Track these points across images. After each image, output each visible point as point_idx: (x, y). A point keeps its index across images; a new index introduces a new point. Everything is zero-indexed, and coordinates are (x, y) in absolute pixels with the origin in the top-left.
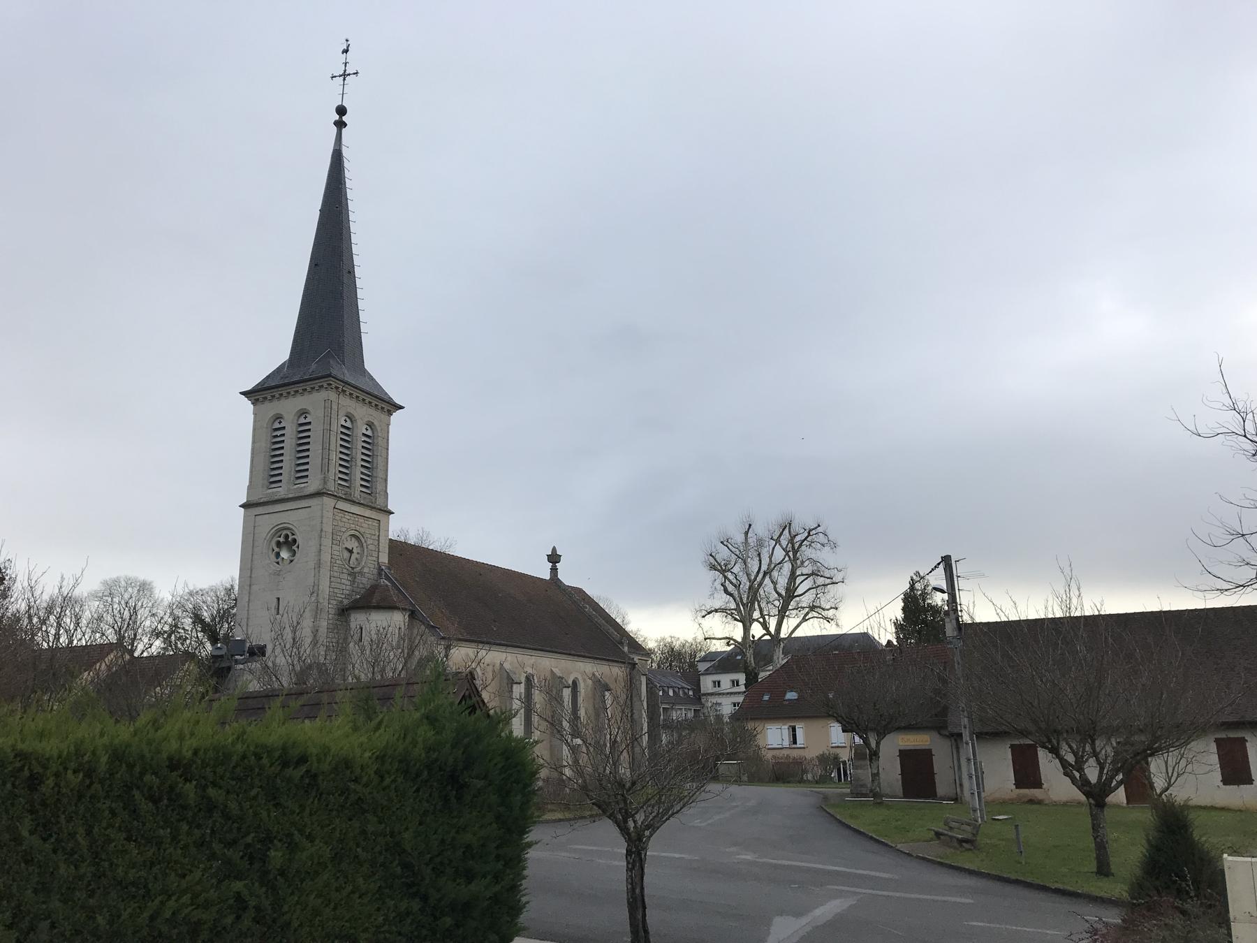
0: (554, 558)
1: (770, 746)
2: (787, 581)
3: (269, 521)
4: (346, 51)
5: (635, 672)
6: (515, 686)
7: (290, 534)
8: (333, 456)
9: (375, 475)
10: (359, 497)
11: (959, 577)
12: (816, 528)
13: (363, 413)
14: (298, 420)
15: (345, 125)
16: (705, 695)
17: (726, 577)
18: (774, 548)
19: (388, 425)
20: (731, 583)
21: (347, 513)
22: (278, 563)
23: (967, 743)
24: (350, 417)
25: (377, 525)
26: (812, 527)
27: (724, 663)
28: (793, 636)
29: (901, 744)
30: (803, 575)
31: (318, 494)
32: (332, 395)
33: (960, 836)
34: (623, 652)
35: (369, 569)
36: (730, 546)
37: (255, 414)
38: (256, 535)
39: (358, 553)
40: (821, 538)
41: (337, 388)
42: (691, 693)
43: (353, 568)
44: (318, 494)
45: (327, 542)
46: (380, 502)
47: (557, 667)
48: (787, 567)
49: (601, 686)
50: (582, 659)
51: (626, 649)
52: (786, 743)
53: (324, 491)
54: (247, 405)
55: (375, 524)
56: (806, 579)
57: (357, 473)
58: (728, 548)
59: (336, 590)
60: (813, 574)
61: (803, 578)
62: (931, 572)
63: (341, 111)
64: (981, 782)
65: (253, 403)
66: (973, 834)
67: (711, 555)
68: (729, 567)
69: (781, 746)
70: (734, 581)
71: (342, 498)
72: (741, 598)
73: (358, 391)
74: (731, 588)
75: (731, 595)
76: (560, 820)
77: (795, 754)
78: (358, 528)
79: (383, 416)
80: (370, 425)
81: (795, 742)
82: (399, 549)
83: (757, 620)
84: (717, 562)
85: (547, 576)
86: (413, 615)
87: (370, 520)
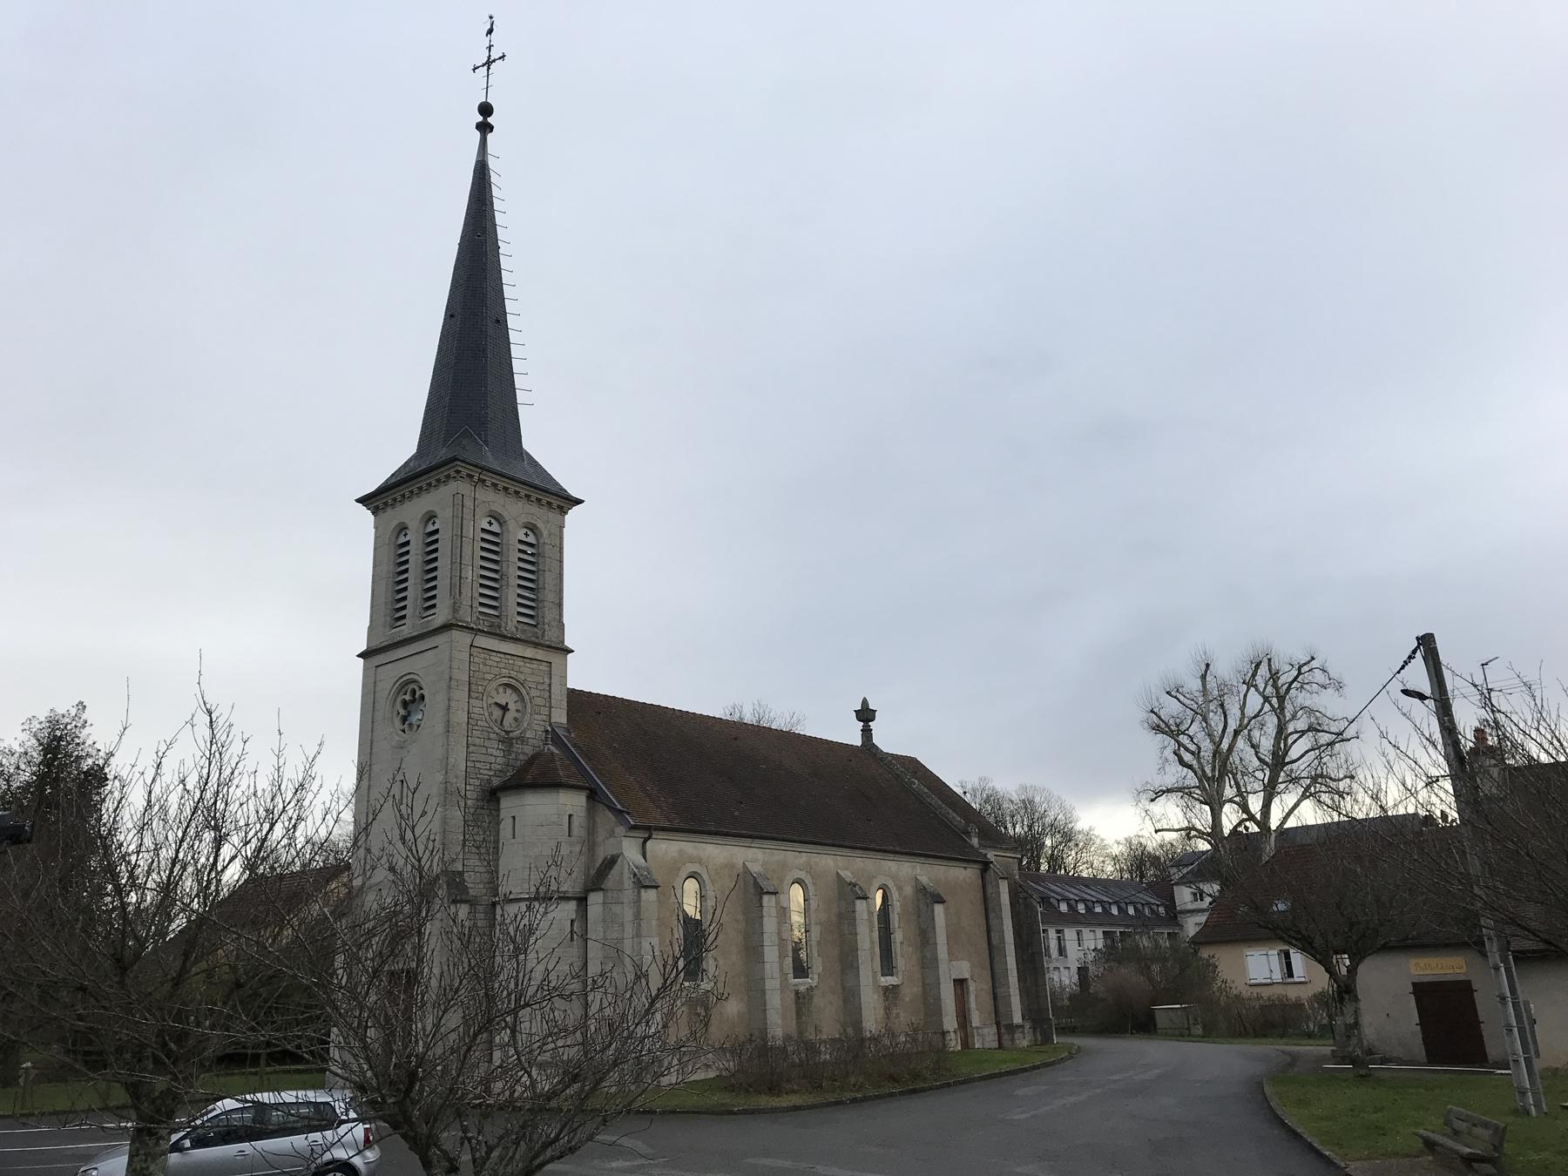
0: (865, 715)
1: (1252, 981)
2: (1272, 741)
3: (391, 675)
4: (490, 32)
5: (990, 875)
6: (766, 898)
7: (417, 689)
8: (468, 573)
9: (541, 598)
10: (514, 629)
11: (1491, 690)
12: (1309, 662)
13: (516, 511)
14: (425, 528)
15: (491, 128)
16: (1182, 912)
17: (1180, 744)
18: (1245, 696)
19: (562, 527)
20: (1187, 750)
21: (494, 654)
22: (404, 731)
23: (1497, 969)
24: (495, 517)
25: (548, 669)
26: (1303, 662)
27: (1199, 868)
28: (1285, 826)
29: (1413, 972)
30: (1296, 732)
31: (446, 627)
32: (463, 487)
33: (1468, 1150)
34: (973, 847)
35: (533, 731)
36: (1182, 698)
37: (376, 528)
38: (377, 695)
39: (518, 711)
40: (1319, 676)
41: (471, 476)
42: (1161, 910)
43: (507, 732)
44: (446, 627)
45: (461, 695)
46: (550, 636)
47: (847, 869)
48: (1271, 722)
49: (929, 897)
50: (892, 856)
51: (975, 841)
52: (1277, 976)
53: (453, 622)
54: (366, 516)
55: (544, 667)
56: (1301, 737)
57: (511, 597)
58: (1178, 699)
59: (478, 765)
60: (1311, 729)
61: (1296, 736)
62: (1403, 668)
63: (486, 109)
64: (1530, 1040)
65: (373, 513)
66: (1494, 1146)
67: (1152, 711)
68: (1183, 728)
69: (1269, 981)
70: (1193, 748)
71: (484, 632)
72: (1203, 771)
73: (503, 479)
74: (1187, 757)
75: (1190, 767)
76: (796, 1108)
77: (1292, 993)
78: (513, 674)
79: (551, 515)
80: (532, 528)
81: (1290, 974)
82: (581, 702)
83: (1231, 801)
84: (1163, 721)
85: (857, 741)
86: (593, 795)
87: (535, 662)
